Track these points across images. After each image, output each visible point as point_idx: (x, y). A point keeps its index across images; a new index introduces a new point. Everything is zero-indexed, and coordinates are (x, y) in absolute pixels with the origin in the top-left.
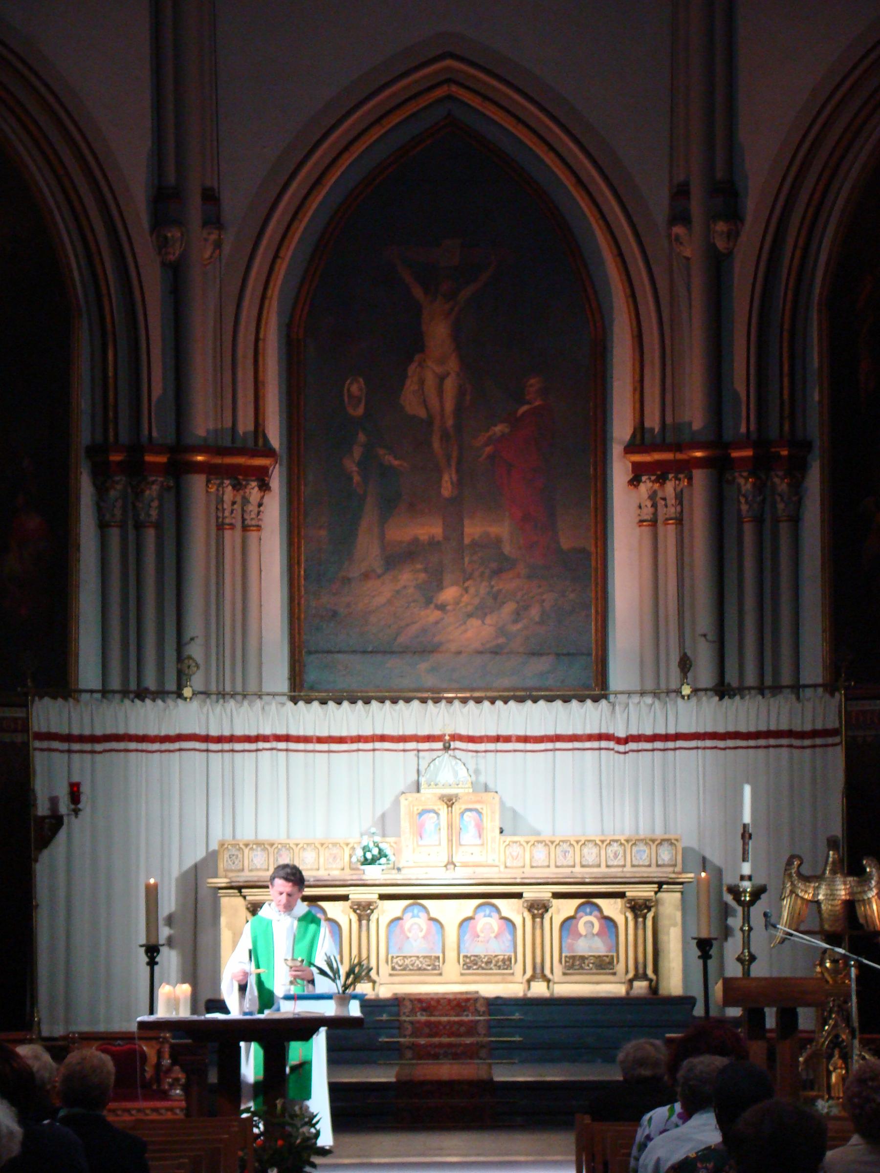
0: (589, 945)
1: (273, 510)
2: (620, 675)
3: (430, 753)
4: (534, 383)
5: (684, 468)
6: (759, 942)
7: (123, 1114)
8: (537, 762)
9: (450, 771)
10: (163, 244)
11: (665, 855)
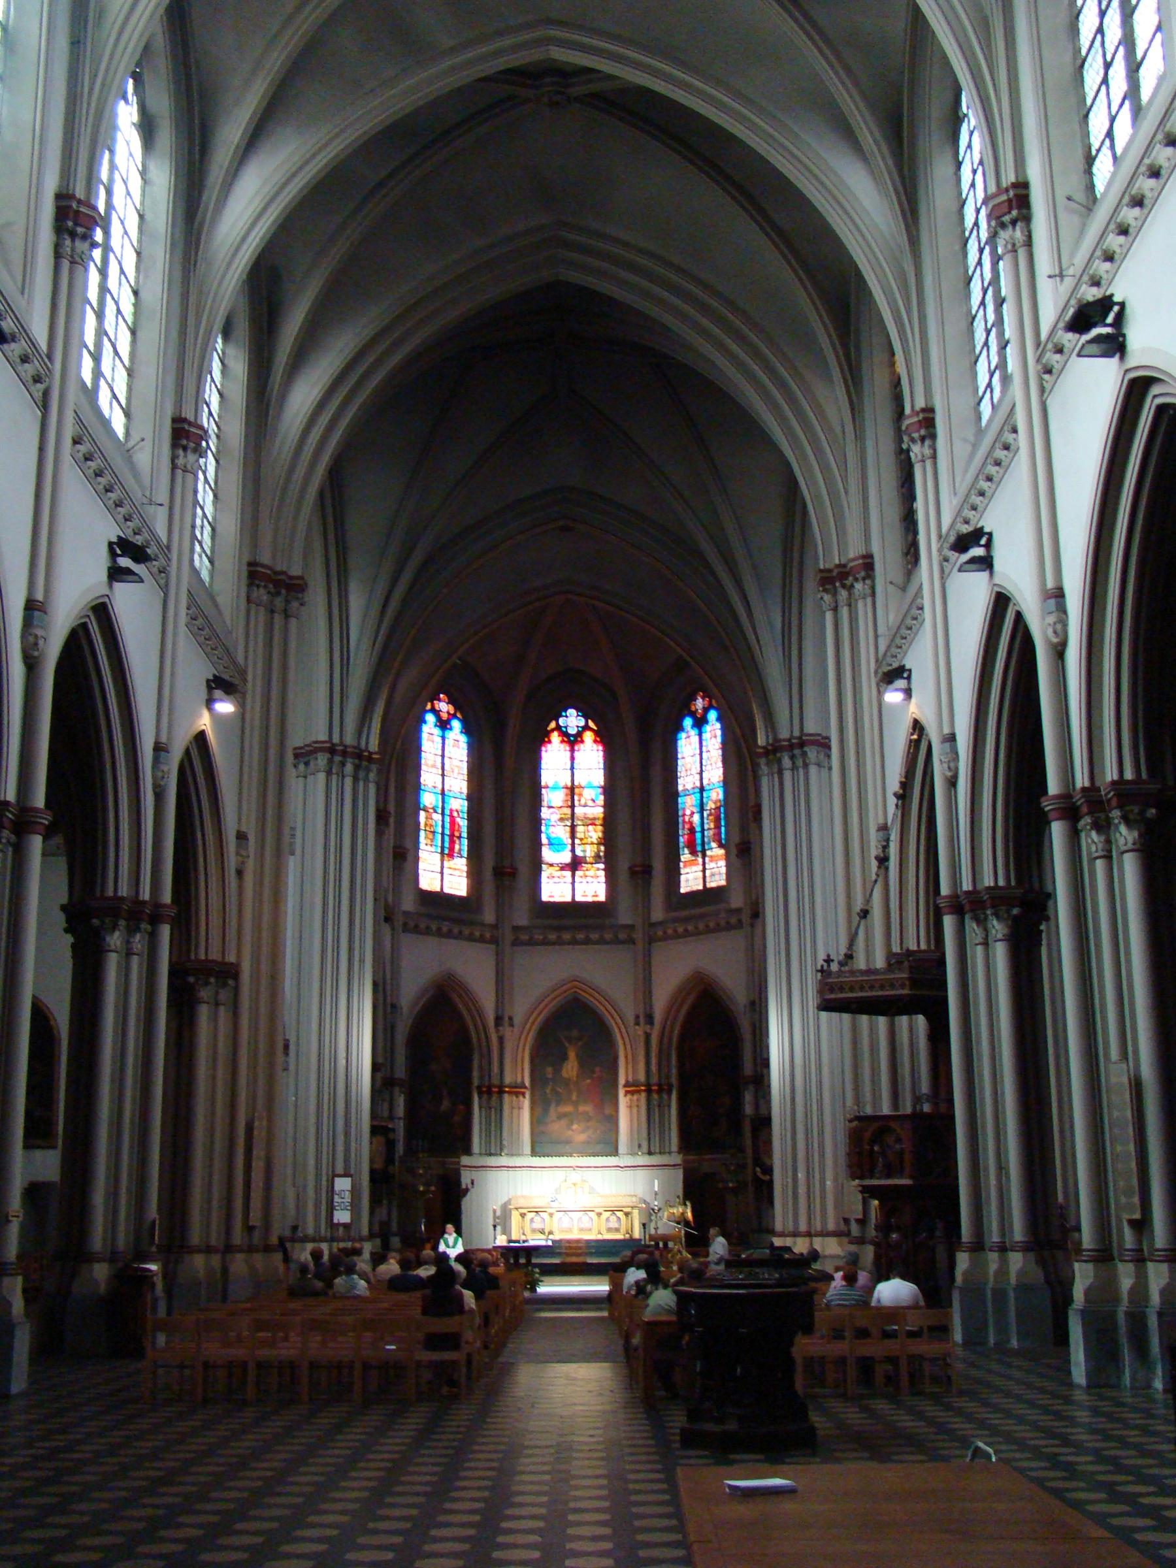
0: (613, 1224)
1: (526, 1103)
2: (622, 1148)
3: (570, 1172)
4: (597, 1069)
5: (638, 1092)
6: (660, 1224)
7: (492, 1270)
8: (599, 1173)
9: (575, 1176)
10: (497, 1031)
11: (634, 1199)
